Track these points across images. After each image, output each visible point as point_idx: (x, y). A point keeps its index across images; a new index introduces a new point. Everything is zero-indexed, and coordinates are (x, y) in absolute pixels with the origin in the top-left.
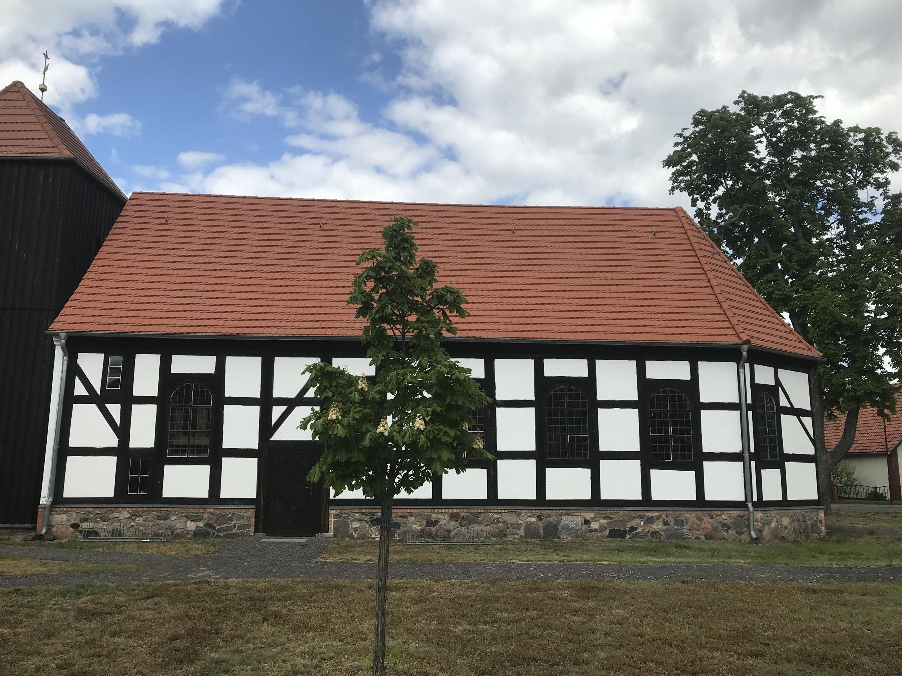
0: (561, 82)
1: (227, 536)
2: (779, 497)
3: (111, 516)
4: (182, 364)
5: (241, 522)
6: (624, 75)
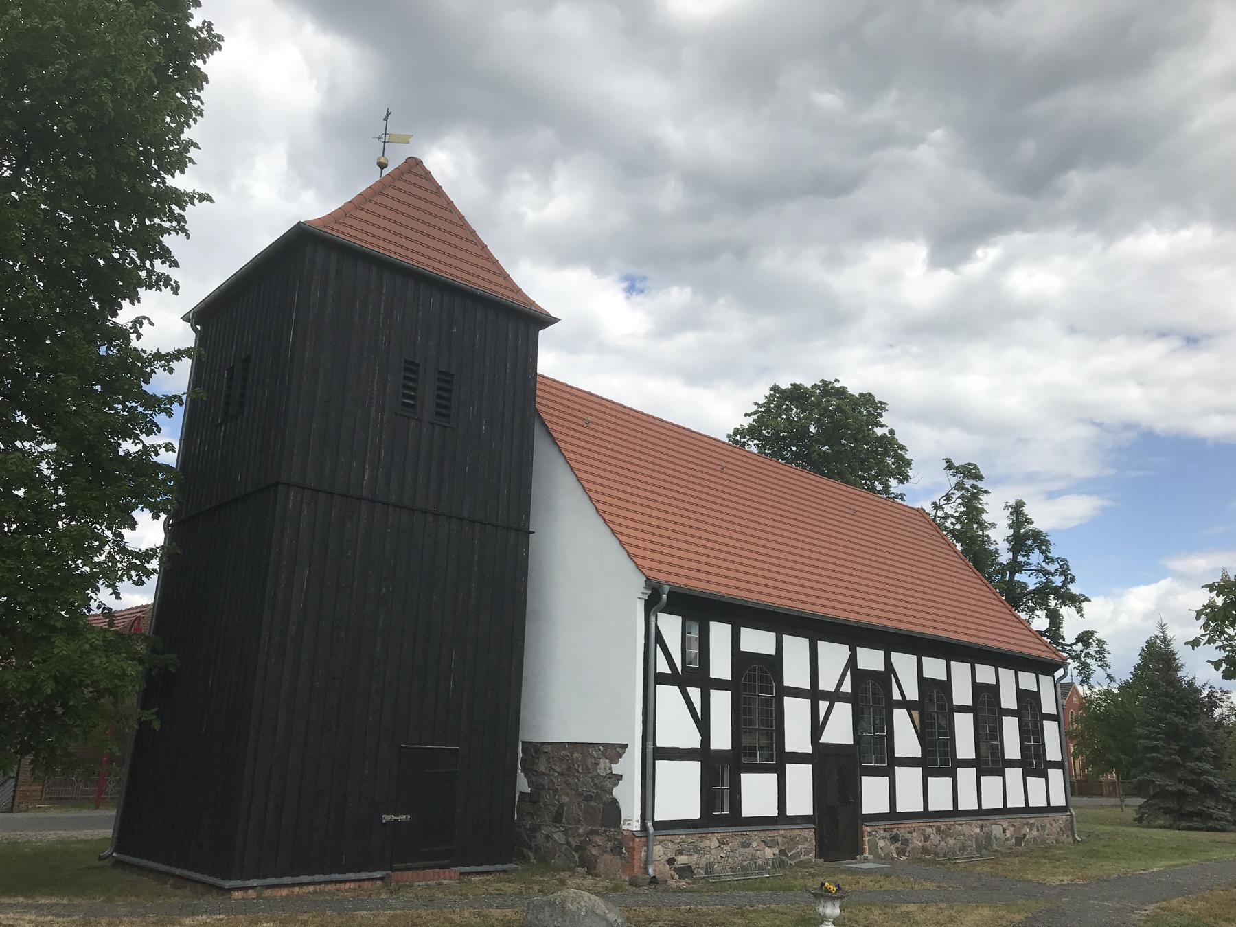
1: (797, 865)
2: (949, 807)
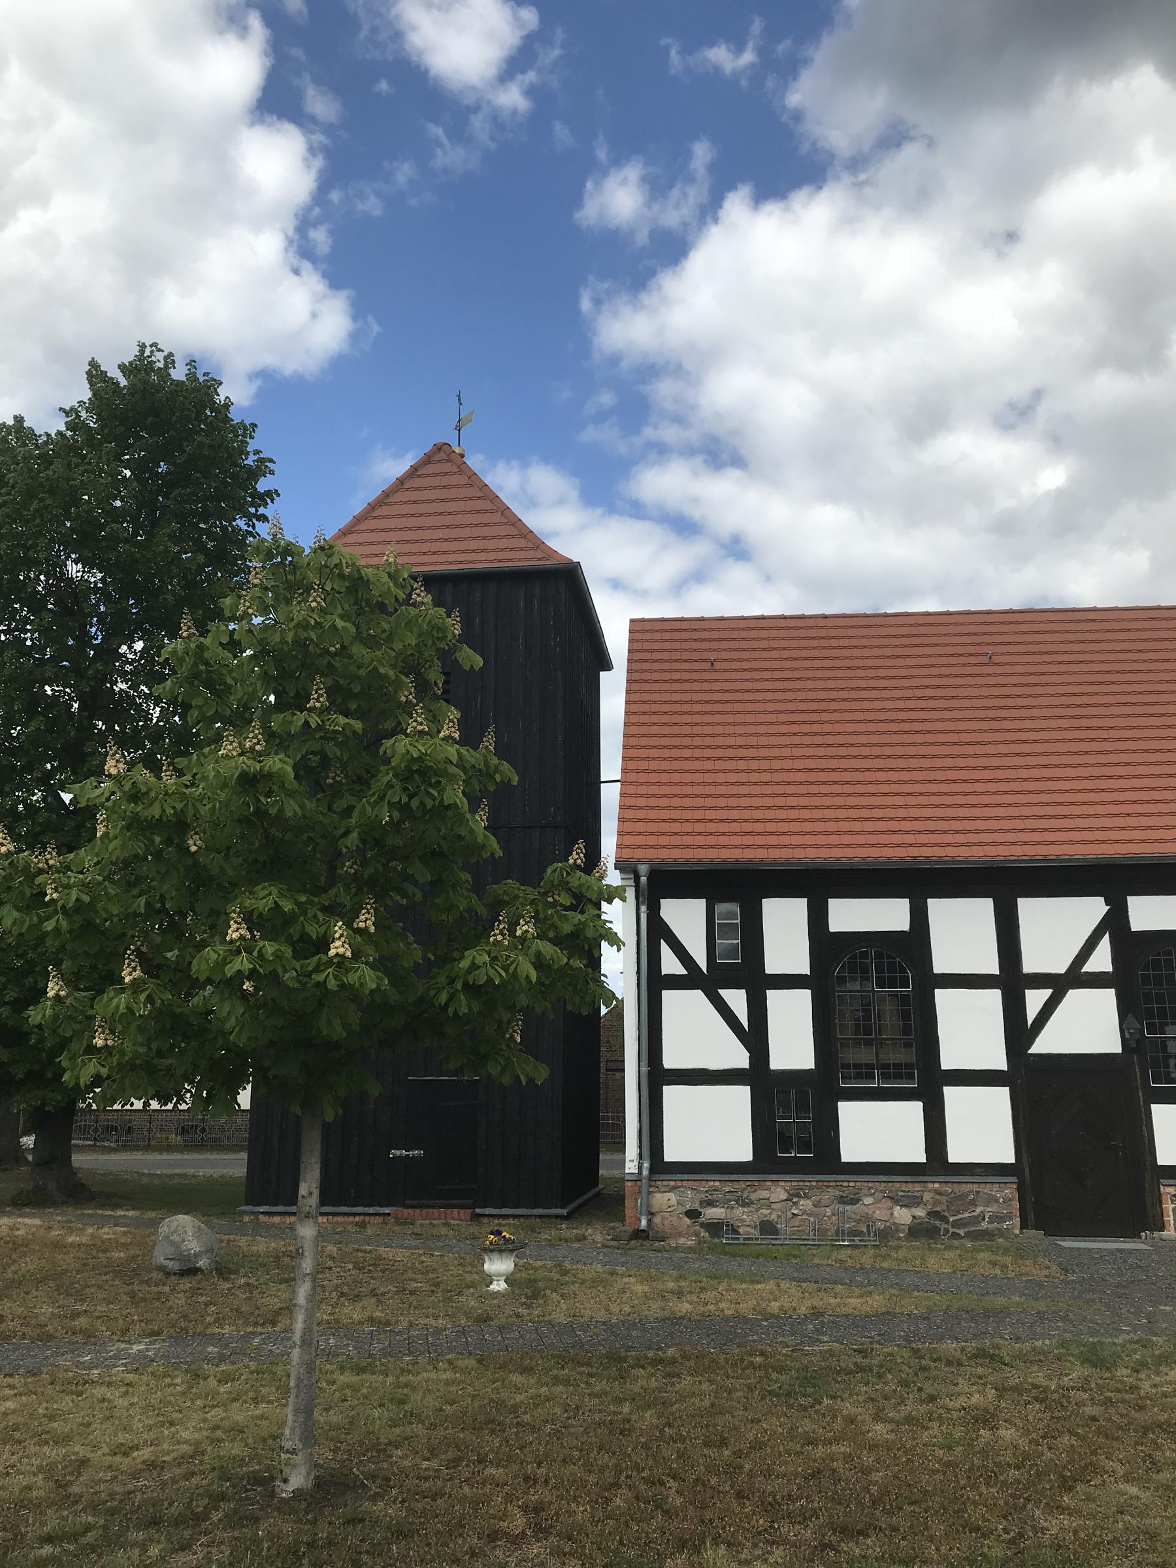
0: (926, 416)
3: (753, 1196)
4: (850, 915)
5: (992, 1209)
6: (1038, 395)
